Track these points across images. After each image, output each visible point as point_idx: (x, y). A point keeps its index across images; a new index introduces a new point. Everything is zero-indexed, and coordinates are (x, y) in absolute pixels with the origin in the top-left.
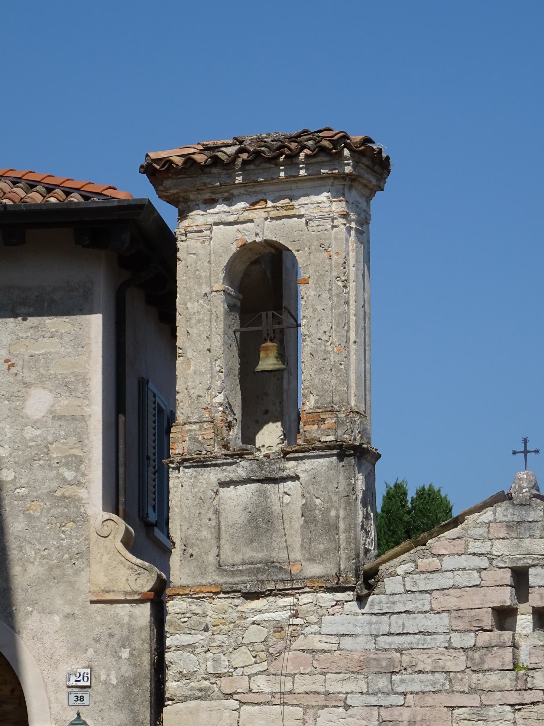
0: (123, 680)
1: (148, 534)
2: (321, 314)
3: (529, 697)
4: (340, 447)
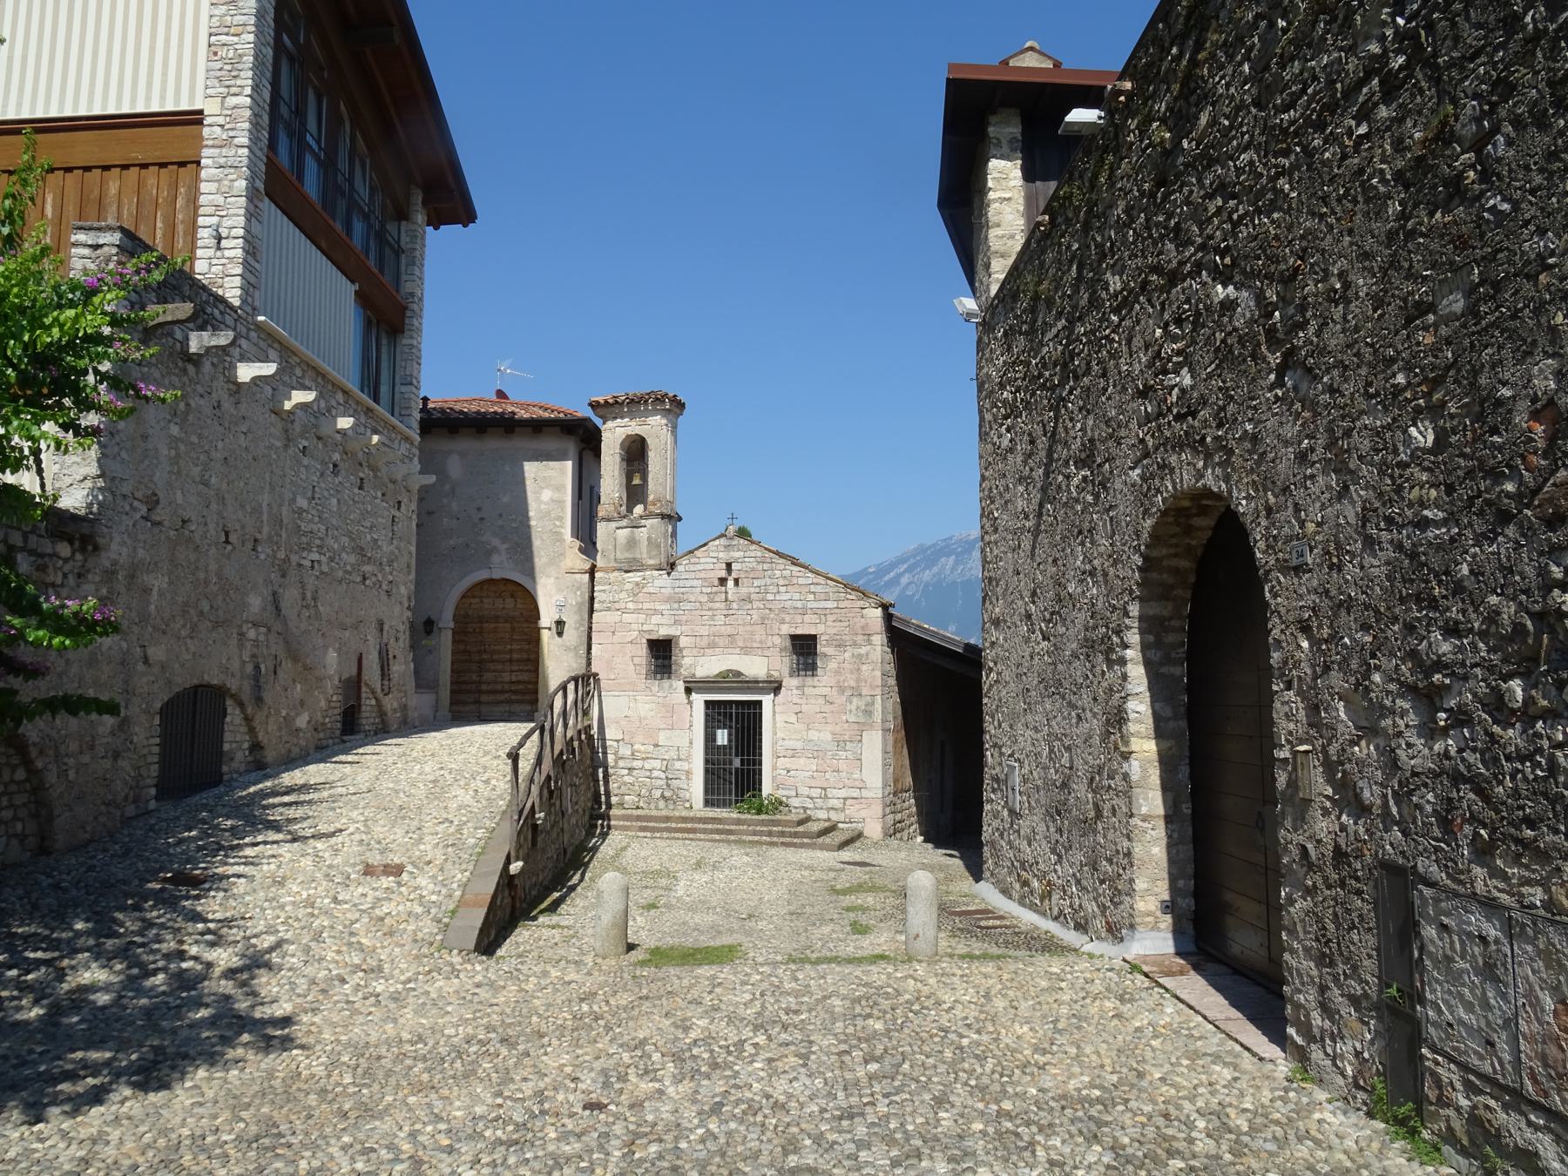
1: (588, 543)
2: (656, 462)
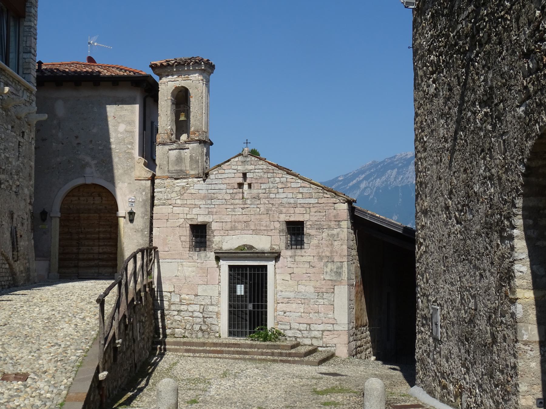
0: (143, 200)
1: (150, 161)
3: (246, 206)
4: (199, 141)
